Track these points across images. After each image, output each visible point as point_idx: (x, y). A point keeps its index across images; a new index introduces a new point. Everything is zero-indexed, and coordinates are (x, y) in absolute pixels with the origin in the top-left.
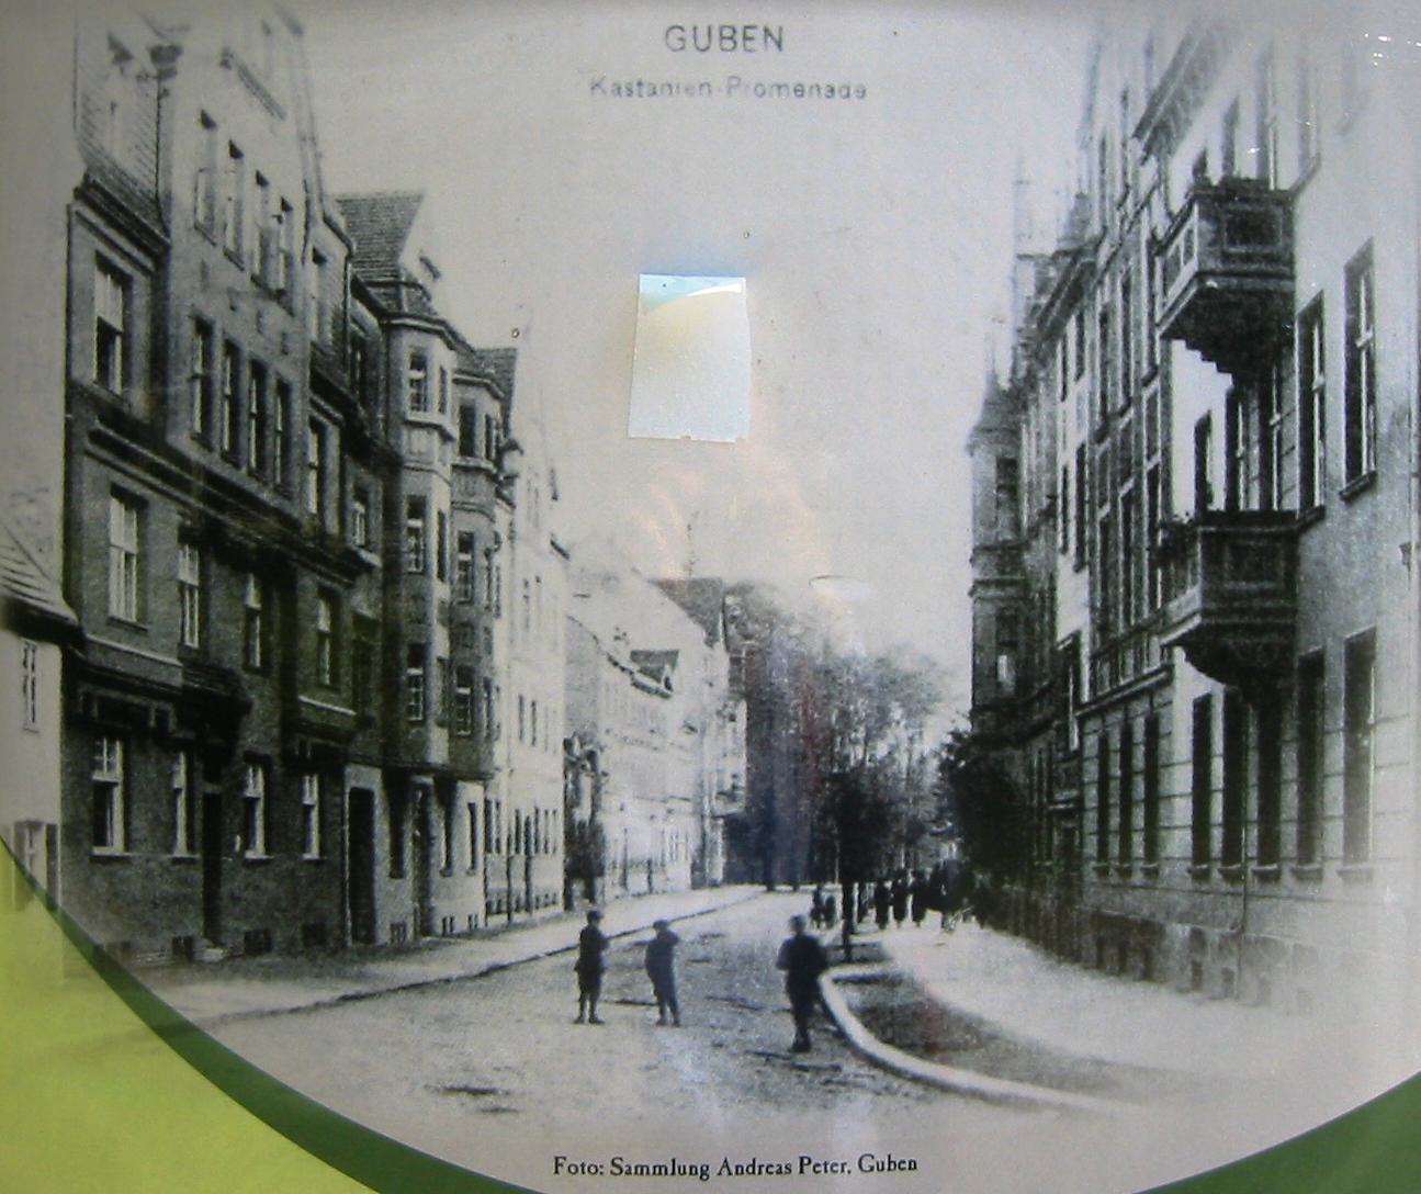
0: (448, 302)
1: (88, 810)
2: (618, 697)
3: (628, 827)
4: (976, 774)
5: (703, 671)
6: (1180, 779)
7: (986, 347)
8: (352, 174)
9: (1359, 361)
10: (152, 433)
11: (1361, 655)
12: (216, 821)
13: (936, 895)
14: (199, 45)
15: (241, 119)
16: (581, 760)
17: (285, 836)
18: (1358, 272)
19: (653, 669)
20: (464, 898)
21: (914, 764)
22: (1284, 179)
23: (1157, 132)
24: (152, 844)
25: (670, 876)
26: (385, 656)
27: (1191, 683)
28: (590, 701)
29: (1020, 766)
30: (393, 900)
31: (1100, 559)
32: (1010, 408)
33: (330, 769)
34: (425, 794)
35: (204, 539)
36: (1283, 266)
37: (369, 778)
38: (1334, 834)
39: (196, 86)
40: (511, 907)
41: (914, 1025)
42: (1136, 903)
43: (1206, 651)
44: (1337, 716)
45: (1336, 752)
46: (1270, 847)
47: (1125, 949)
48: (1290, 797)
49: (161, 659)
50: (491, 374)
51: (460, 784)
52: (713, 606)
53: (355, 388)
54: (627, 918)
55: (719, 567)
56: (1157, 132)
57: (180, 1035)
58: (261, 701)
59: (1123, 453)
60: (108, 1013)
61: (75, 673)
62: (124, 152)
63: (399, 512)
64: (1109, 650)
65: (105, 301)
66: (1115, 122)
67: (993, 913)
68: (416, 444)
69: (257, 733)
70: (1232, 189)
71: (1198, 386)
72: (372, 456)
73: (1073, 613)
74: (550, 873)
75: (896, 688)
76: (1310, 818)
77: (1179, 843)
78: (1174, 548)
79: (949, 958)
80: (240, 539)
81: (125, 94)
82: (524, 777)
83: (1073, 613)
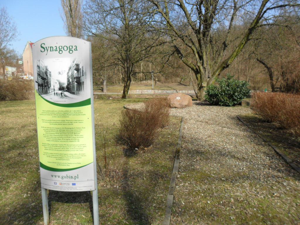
0: (49, 70)
1: (39, 89)
2: (55, 84)
3: (56, 89)
4: (67, 87)
5: (58, 83)
6: (75, 88)
7: (67, 71)
8: (46, 65)
9: (83, 71)
10: (40, 75)
11: (83, 82)
12: (43, 89)
13: (66, 91)
14: (40, 60)
15: (42, 63)
16: (54, 86)
17: (45, 89)
18: (82, 67)
19: (56, 83)
20: (50, 91)
21: (291, 159)
22: (79, 63)
23: (73, 62)
24: (41, 90)
25: (57, 91)
26: (47, 82)
27: (76, 83)
28: (54, 85)
29: (69, 86)
30: (48, 92)
31: (72, 78)
32: (68, 73)
33: (46, 87)
34: (49, 88)
35: (42, 78)
36: (79, 67)
37: (47, 87)
38: (82, 89)
39: (41, 62)
40: (52, 92)
41: (66, 96)
42: (74, 92)
43: (76, 82)
44: (82, 85)
45: (82, 86)
46: (79, 90)
47: (73, 93)
48: (80, 88)
49: (40, 83)
50: (50, 72)
51: (6, 67)
52: (58, 80)
53: (46, 73)
54: (56, 92)
55: (58, 79)
56: (73, 62)
57: (42, 97)
58: (44, 84)
59: (72, 75)
60: (40, 96)
61: (38, 84)
62: (38, 64)
63: (48, 77)
64: (72, 82)
65: (38, 70)
66: (72, 62)
67: (68, 92)
68: (48, 75)
69: (44, 86)
70: (77, 64)
71: (76, 72)
72: (47, 75)
73: (71, 81)
74: (53, 90)
75: (64, 84)
76: (81, 89)
77: (75, 89)
78: (75, 78)
79: (67, 93)
80: (43, 79)
81: (38, 62)
82: (52, 87)
83: (71, 81)
